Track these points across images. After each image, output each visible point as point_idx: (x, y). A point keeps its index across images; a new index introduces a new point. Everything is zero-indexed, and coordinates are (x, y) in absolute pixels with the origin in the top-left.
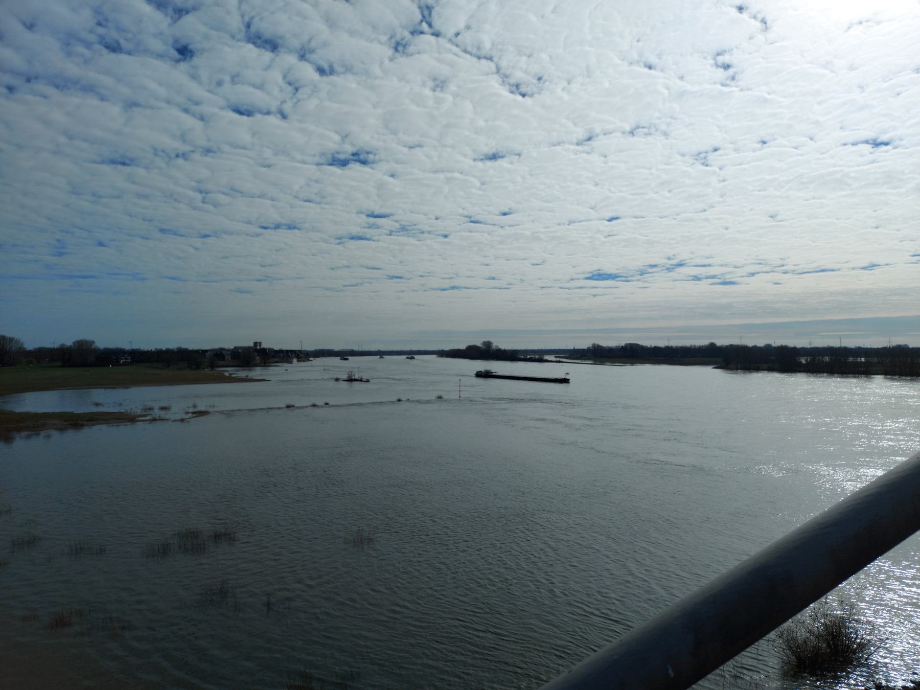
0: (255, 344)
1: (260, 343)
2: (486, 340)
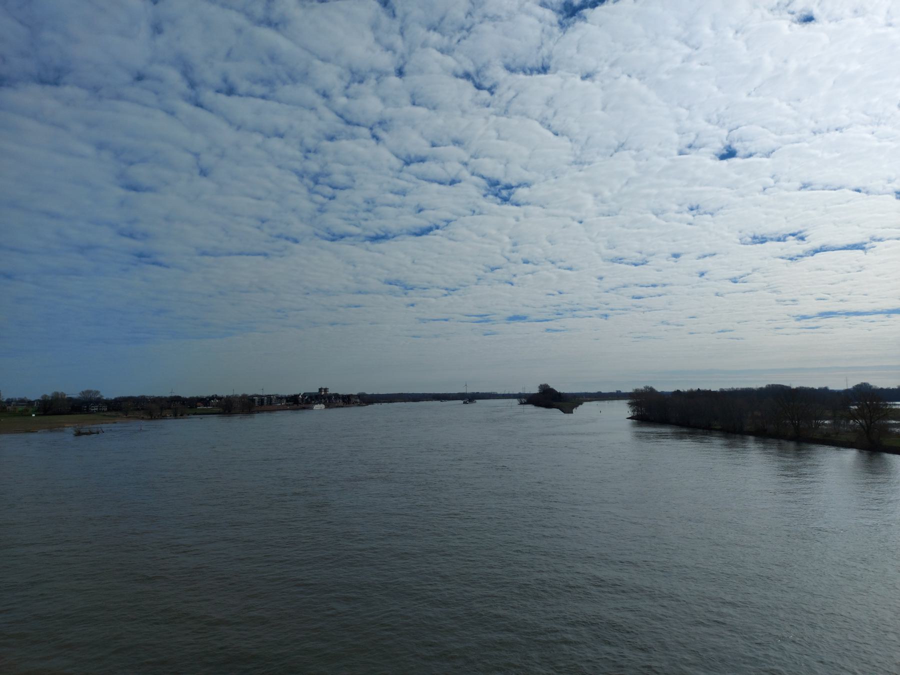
0: (320, 390)
1: (326, 390)
2: (543, 383)
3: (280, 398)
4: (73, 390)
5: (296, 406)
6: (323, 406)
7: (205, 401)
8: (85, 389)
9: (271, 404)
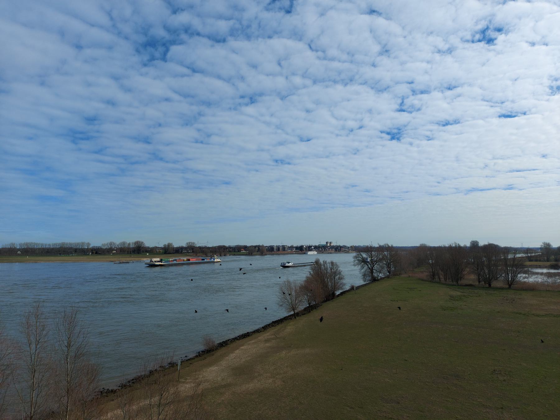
0: (327, 243)
1: (330, 243)
2: (474, 240)
3: (292, 247)
6: (315, 253)
7: (245, 248)
9: (284, 250)
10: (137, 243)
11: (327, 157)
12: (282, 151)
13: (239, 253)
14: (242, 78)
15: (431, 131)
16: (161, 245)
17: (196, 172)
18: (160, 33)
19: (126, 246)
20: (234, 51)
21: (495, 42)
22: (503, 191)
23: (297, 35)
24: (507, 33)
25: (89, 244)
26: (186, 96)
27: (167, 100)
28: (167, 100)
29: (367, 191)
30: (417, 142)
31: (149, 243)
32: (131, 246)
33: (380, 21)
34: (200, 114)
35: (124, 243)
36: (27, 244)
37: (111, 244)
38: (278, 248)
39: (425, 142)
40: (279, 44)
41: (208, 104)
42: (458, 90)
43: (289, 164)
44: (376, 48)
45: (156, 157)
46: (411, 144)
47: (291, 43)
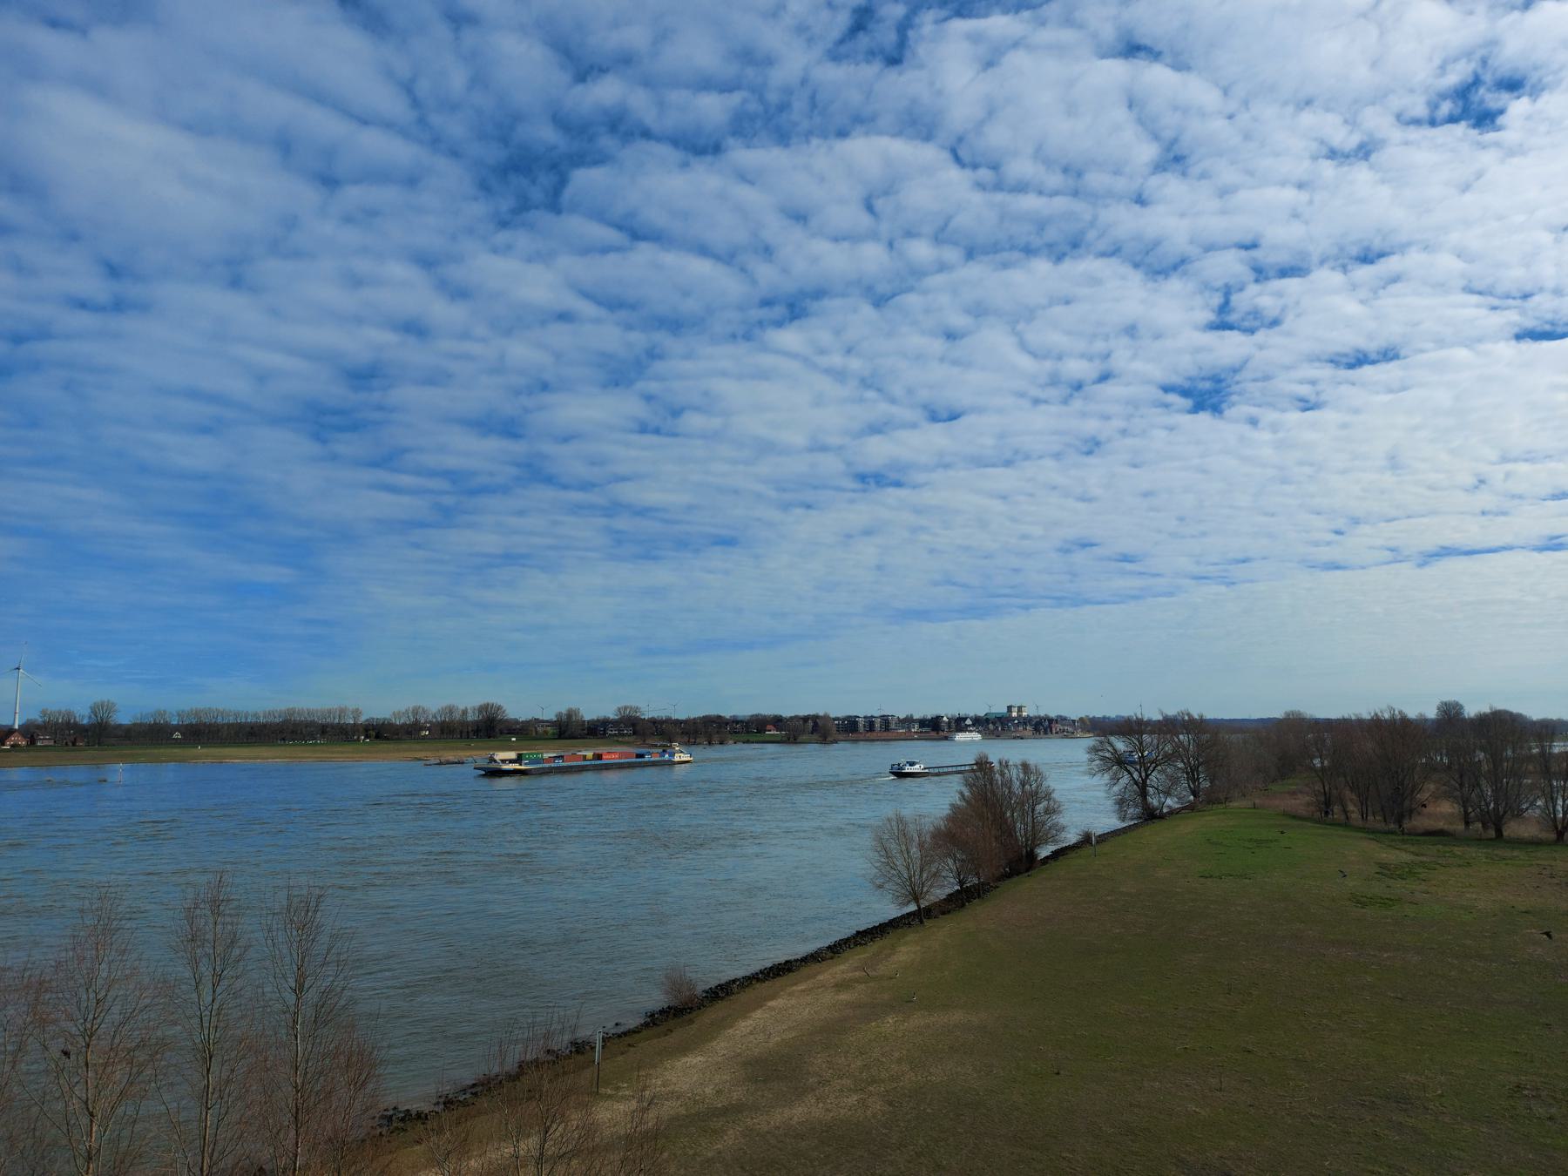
0: (1010, 708)
2: (1449, 698)
3: (908, 721)
4: (597, 706)
5: (934, 734)
6: (977, 736)
7: (778, 721)
8: (1289, 709)
10: (484, 708)
11: (1008, 463)
12: (878, 451)
13: (759, 737)
14: (767, 251)
15: (1313, 383)
16: (549, 715)
17: (643, 512)
18: (546, 135)
19: (457, 716)
20: (744, 177)
21: (1500, 120)
22: (1535, 554)
23: (918, 124)
24: (1536, 92)
25: (357, 712)
26: (613, 304)
27: (564, 317)
28: (564, 317)
29: (1126, 558)
30: (1269, 416)
31: (518, 708)
32: (470, 718)
33: (1157, 77)
34: (653, 354)
35: (451, 710)
36: (197, 713)
37: (416, 711)
38: (870, 723)
39: (1294, 416)
40: (868, 152)
41: (675, 325)
42: (1392, 264)
43: (898, 484)
44: (1147, 152)
45: (535, 472)
46: (1253, 422)
47: (902, 149)
